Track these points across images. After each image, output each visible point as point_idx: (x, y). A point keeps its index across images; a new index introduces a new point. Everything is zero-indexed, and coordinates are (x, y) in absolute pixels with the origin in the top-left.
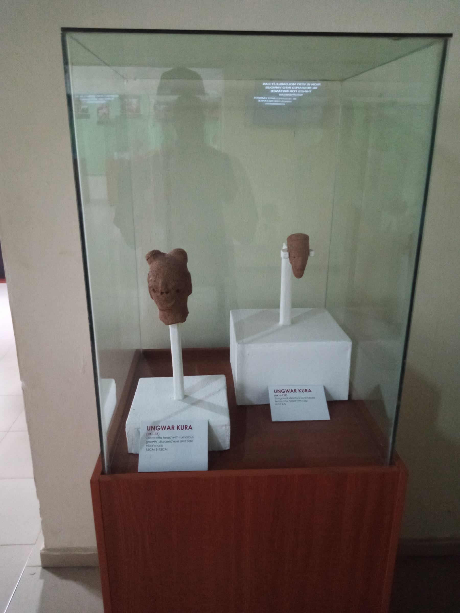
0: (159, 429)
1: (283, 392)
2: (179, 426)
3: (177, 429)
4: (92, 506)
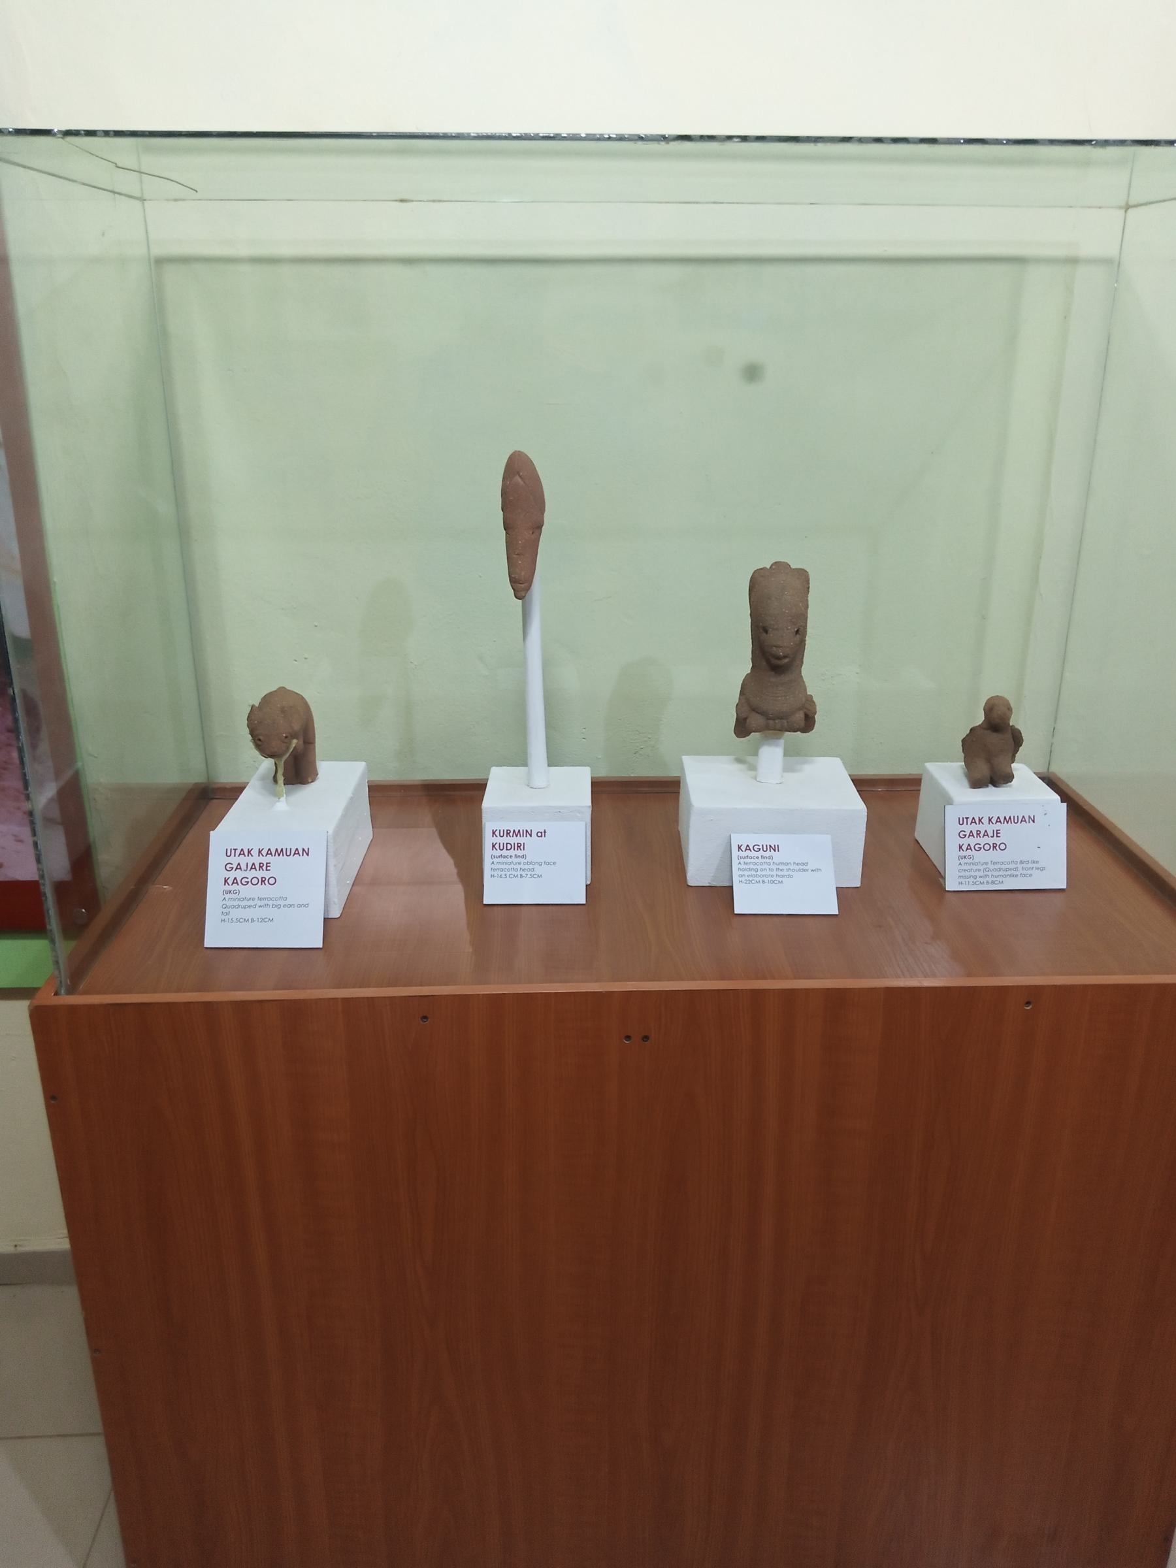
1: (244, 883)
2: (992, 818)
4: (35, 1053)
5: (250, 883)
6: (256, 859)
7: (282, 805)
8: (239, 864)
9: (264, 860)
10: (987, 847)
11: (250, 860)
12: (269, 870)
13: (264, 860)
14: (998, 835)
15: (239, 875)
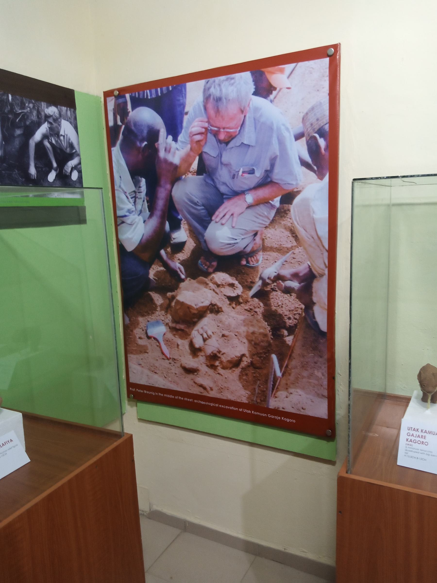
1: (415, 442)
5: (417, 443)
6: (421, 434)
7: (428, 412)
8: (413, 434)
9: (424, 434)
10: (419, 442)
11: (418, 433)
12: (425, 439)
13: (424, 434)
14: (425, 438)
15: (413, 438)
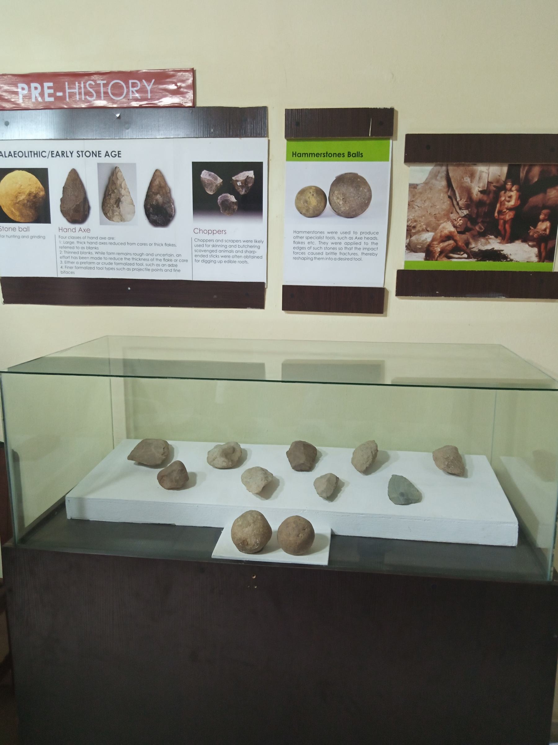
0: (115, 156)
3: (73, 152)
14: (100, 155)
